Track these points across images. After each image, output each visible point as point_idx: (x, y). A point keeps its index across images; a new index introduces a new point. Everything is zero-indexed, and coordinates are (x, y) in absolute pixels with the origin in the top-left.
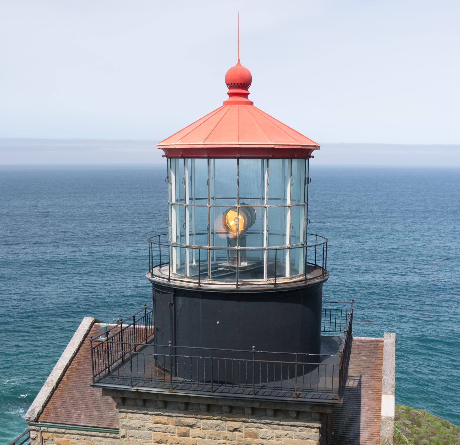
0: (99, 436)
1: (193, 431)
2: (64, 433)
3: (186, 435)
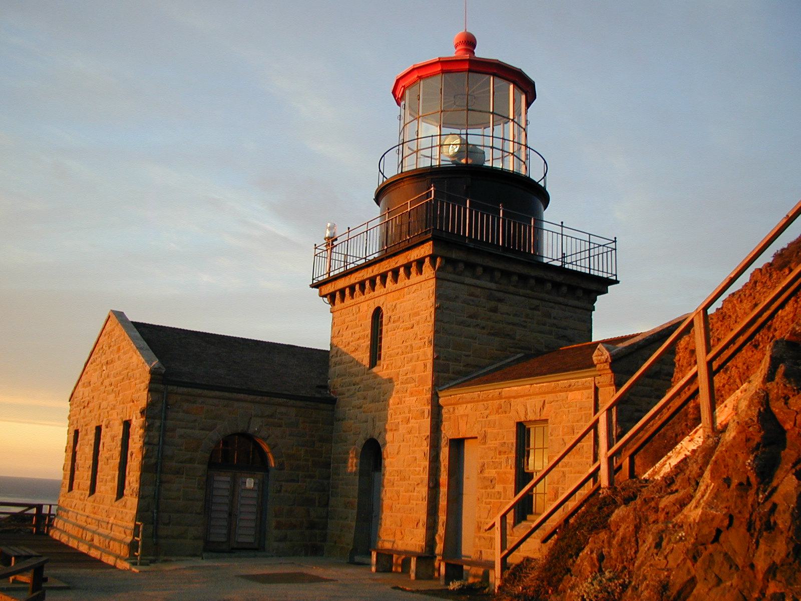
0: (246, 401)
1: (503, 308)
2: (200, 396)
3: (495, 310)
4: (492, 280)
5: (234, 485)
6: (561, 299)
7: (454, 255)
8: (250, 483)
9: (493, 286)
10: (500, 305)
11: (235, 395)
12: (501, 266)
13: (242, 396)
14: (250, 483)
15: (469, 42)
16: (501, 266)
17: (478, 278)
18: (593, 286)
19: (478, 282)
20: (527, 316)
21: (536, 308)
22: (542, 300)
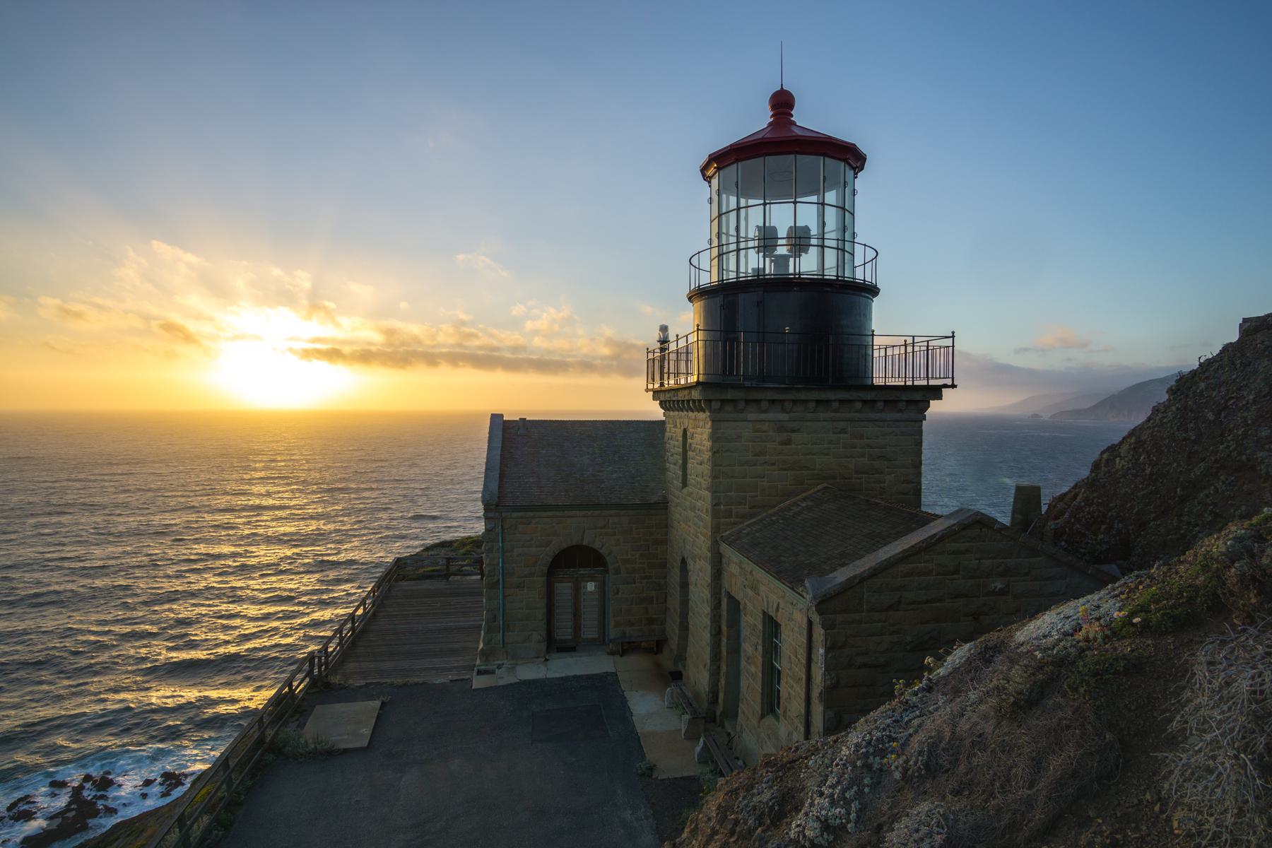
3: (788, 442)
4: (784, 411)
5: (577, 590)
6: (878, 416)
7: (729, 395)
8: (591, 586)
9: (784, 417)
10: (794, 435)
11: (566, 513)
12: (791, 397)
13: (573, 513)
14: (591, 586)
15: (782, 103)
16: (791, 397)
17: (765, 412)
18: (918, 396)
19: (763, 416)
20: (830, 442)
21: (843, 431)
22: (852, 420)
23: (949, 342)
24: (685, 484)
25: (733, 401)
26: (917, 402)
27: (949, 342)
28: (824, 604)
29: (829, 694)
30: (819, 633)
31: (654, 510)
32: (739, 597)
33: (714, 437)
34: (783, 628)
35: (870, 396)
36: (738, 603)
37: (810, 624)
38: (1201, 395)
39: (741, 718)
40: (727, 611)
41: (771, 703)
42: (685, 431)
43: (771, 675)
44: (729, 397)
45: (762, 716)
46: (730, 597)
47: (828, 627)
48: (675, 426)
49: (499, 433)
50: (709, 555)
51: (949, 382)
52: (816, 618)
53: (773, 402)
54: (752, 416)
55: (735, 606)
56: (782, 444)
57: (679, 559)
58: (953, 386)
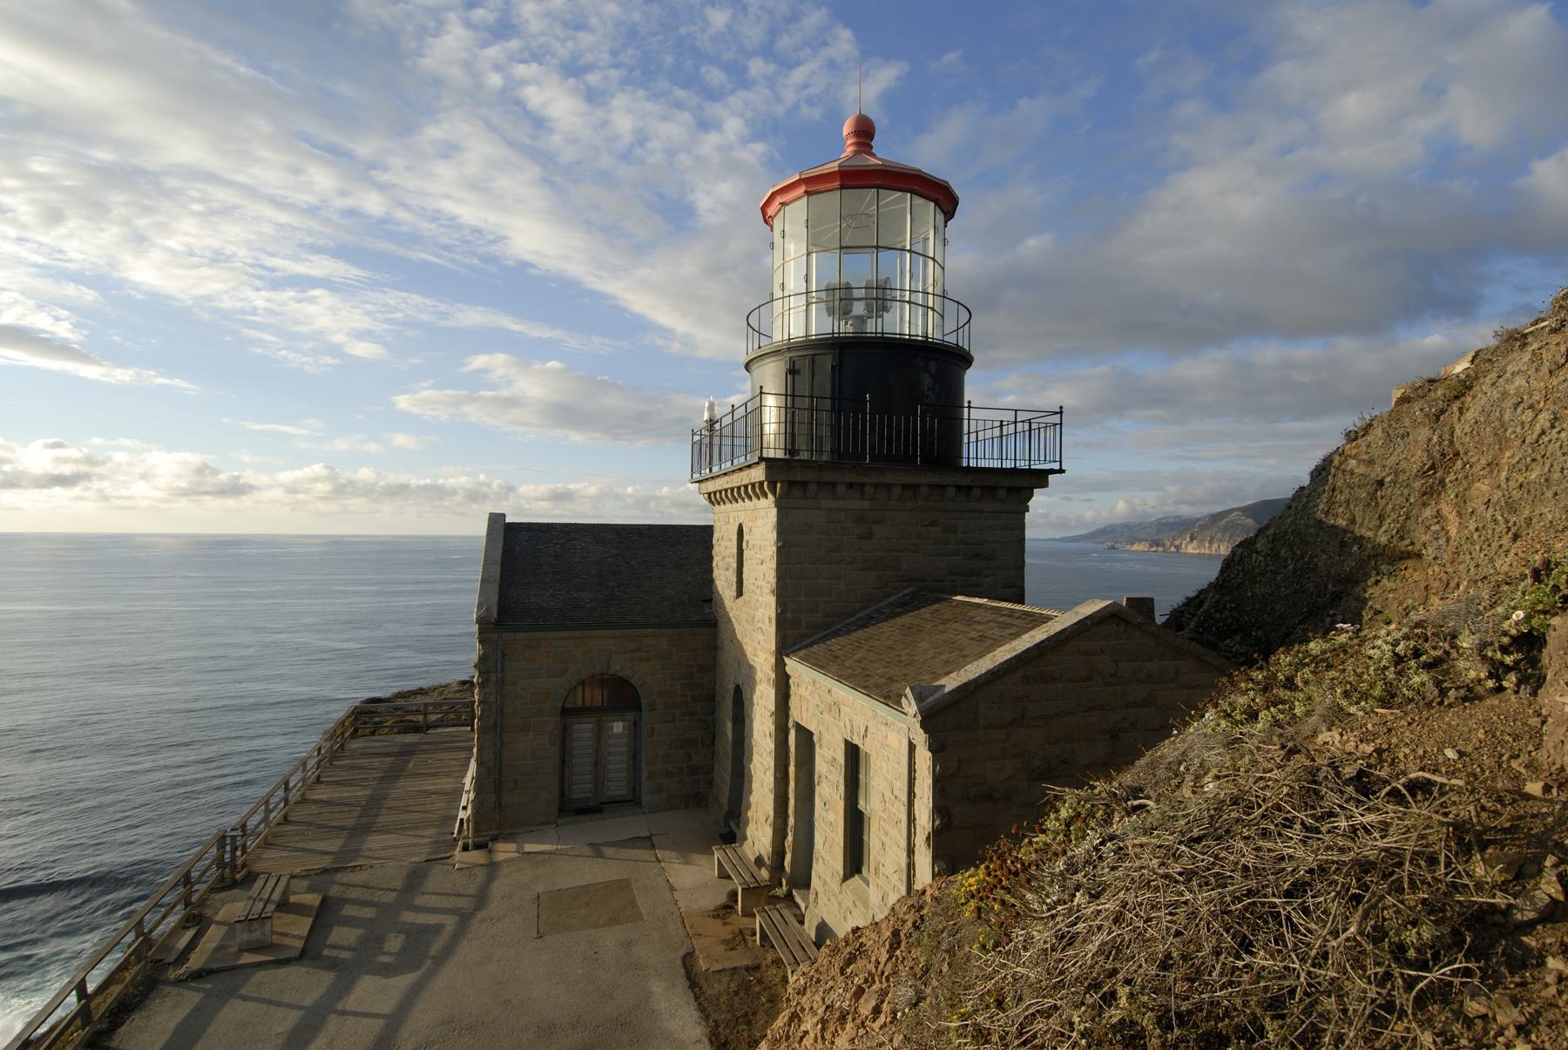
3: (868, 536)
5: (599, 734)
7: (799, 476)
8: (618, 727)
9: (865, 504)
14: (618, 727)
23: (1056, 419)
24: (740, 593)
25: (804, 485)
26: (1019, 490)
27: (1056, 419)
28: (931, 719)
29: (938, 840)
30: (924, 758)
31: (701, 617)
32: (811, 728)
33: (783, 528)
34: (873, 759)
35: (966, 481)
36: (811, 734)
37: (912, 748)
38: (1352, 472)
39: (815, 882)
40: (798, 749)
41: (855, 860)
42: (741, 526)
43: (855, 823)
44: (799, 478)
45: (846, 878)
46: (799, 727)
47: (936, 748)
48: (728, 523)
49: (500, 537)
50: (773, 676)
51: (1056, 466)
52: (920, 738)
53: (851, 485)
54: (824, 504)
55: (806, 737)
56: (861, 537)
57: (731, 687)
58: (1061, 471)
